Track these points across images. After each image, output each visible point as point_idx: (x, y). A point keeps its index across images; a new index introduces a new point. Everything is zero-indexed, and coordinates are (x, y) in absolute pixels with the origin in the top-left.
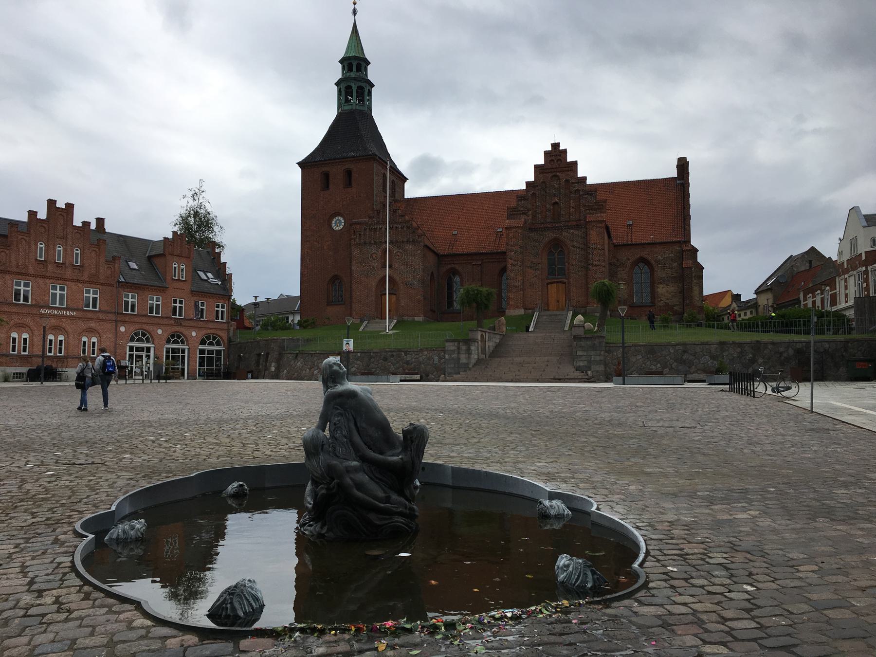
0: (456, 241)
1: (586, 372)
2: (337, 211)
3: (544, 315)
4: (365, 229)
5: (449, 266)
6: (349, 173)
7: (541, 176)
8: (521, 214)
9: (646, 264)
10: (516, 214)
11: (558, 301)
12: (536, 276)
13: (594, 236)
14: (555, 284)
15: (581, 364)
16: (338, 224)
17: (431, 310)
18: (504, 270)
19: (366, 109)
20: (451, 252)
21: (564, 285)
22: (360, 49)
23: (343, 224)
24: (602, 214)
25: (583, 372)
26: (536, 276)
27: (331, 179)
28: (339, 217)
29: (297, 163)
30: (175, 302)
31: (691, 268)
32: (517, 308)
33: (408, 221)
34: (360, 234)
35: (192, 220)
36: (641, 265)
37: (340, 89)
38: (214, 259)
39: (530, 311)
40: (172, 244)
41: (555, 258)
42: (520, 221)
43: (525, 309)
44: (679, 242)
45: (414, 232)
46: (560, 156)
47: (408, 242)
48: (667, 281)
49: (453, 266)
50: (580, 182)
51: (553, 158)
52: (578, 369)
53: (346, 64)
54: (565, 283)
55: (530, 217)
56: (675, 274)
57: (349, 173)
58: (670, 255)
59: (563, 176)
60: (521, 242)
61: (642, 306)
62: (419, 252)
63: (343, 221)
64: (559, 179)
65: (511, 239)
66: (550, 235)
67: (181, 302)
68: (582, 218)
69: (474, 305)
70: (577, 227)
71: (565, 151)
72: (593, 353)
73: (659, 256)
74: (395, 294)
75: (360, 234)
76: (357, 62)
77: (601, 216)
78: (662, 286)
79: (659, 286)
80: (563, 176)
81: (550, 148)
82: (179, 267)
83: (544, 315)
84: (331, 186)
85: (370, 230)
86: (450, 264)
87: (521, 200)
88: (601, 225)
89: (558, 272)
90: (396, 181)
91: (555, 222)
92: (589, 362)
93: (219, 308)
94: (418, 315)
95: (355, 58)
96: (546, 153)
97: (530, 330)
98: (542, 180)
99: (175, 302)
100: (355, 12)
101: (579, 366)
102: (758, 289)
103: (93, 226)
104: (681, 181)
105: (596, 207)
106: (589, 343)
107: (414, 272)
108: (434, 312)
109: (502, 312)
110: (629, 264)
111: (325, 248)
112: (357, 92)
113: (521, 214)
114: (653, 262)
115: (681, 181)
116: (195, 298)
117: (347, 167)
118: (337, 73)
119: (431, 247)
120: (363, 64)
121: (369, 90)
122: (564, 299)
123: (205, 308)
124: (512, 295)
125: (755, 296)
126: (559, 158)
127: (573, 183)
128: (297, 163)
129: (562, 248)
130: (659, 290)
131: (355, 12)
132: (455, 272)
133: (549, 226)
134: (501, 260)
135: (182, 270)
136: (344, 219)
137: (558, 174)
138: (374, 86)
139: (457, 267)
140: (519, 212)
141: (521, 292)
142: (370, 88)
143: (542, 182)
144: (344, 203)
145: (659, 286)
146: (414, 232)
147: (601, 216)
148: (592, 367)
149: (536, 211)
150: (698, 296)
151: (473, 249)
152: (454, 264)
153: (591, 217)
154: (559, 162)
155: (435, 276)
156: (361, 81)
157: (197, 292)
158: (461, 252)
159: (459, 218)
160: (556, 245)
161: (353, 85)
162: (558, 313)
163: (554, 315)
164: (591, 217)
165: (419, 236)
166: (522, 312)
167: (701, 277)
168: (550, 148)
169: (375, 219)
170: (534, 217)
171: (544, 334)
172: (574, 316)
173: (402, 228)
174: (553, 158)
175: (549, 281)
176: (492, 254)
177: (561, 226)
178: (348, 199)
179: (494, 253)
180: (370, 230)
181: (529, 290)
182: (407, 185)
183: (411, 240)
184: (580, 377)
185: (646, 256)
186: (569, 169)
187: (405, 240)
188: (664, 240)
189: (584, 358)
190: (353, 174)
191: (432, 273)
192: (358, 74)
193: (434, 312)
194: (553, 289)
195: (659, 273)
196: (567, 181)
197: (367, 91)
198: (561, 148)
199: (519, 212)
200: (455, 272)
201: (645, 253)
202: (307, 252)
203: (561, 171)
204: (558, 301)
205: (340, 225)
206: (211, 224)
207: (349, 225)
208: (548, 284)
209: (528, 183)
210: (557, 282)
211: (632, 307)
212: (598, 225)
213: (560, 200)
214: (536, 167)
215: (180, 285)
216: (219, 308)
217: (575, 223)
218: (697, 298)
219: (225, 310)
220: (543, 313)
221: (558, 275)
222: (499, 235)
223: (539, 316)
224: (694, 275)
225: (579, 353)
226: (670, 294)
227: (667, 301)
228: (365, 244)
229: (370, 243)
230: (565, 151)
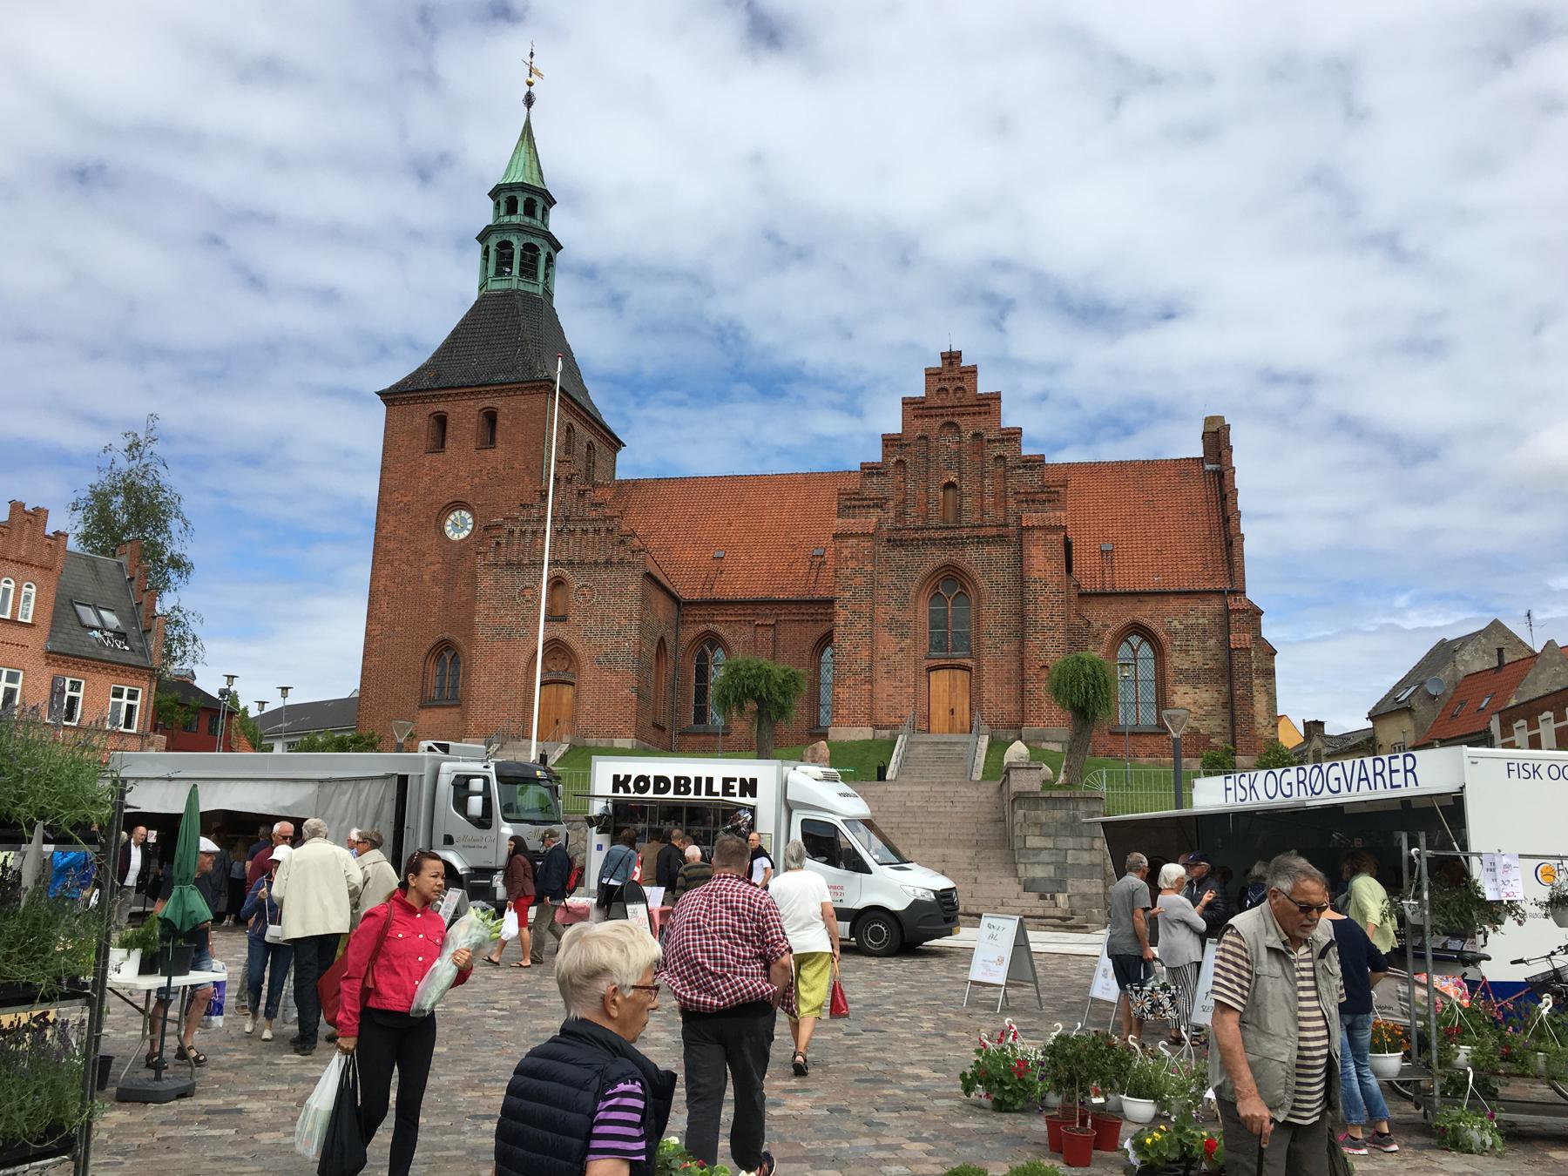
0: (721, 572)
1: (1053, 897)
2: (458, 499)
3: (921, 743)
4: (511, 532)
5: (702, 628)
6: (491, 417)
7: (917, 422)
8: (868, 506)
9: (1145, 639)
10: (859, 507)
11: (952, 711)
12: (902, 650)
13: (1042, 561)
14: (946, 672)
15: (1039, 872)
16: (458, 527)
17: (655, 725)
18: (826, 640)
19: (541, 292)
20: (707, 595)
21: (966, 674)
22: (535, 172)
23: (470, 527)
24: (1058, 514)
25: (1042, 897)
26: (902, 650)
27: (449, 430)
28: (463, 513)
29: (377, 393)
30: (118, 694)
31: (1248, 650)
32: (855, 724)
33: (612, 518)
34: (498, 543)
35: (119, 500)
36: (1135, 640)
37: (488, 247)
38: (131, 579)
39: (886, 733)
40: (53, 543)
41: (947, 610)
42: (869, 521)
43: (877, 727)
44: (1220, 593)
45: (622, 542)
46: (961, 379)
47: (608, 563)
48: (1193, 678)
49: (711, 626)
50: (1008, 440)
51: (945, 385)
52: (1029, 886)
53: (503, 199)
54: (969, 669)
55: (892, 514)
56: (1211, 664)
57: (491, 417)
58: (1200, 621)
59: (967, 425)
60: (869, 568)
61: (1140, 734)
62: (631, 588)
63: (470, 521)
64: (959, 432)
65: (846, 561)
66: (937, 557)
67: (132, 696)
68: (1011, 520)
69: (751, 706)
70: (1001, 539)
71: (973, 371)
72: (1071, 842)
73: (1176, 623)
74: (573, 684)
75: (498, 543)
76: (526, 195)
77: (1053, 516)
78: (1181, 689)
79: (1176, 689)
80: (967, 425)
81: (937, 363)
82: (18, 590)
83: (921, 743)
84: (448, 443)
85: (523, 533)
86: (705, 622)
87: (871, 475)
88: (1055, 537)
89: (952, 641)
90: (596, 444)
91: (948, 528)
92: (1061, 866)
93: (121, 696)
94: (620, 734)
95: (523, 187)
96: (930, 374)
97: (887, 777)
98: (919, 433)
99: (118, 694)
100: (529, 100)
101: (1033, 880)
102: (1375, 708)
103: (731, 791)
104: (1214, 467)
105: (1044, 496)
106: (1060, 814)
107: (619, 633)
108: (663, 729)
109: (817, 733)
110: (1107, 636)
111: (426, 578)
112: (523, 256)
113: (868, 506)
114: (1162, 635)
115: (1214, 467)
116: (54, 670)
117: (487, 403)
118: (484, 213)
119: (660, 576)
120: (540, 203)
121: (549, 254)
122: (967, 706)
123: (80, 695)
124: (844, 693)
125: (1370, 724)
126: (960, 384)
127: (989, 441)
128: (377, 393)
129: (963, 586)
130: (1175, 698)
131: (529, 100)
132: (714, 640)
133: (936, 535)
134: (819, 617)
135: (28, 598)
136: (474, 516)
137: (956, 420)
138: (562, 247)
139: (720, 629)
140: (865, 503)
141: (867, 687)
142: (553, 253)
143: (921, 438)
144: (476, 480)
145: (1176, 689)
146: (622, 542)
147: (1053, 516)
148: (1069, 881)
149: (904, 501)
150: (1265, 714)
151: (760, 590)
152: (713, 622)
153: (1031, 518)
154: (959, 394)
155: (668, 647)
156: (533, 235)
157: (61, 654)
158: (730, 595)
159: (730, 524)
160: (951, 580)
161: (514, 240)
162: (955, 738)
163: (945, 743)
164: (1031, 518)
165: (633, 552)
166: (866, 733)
167: (1270, 673)
168: (938, 363)
169: (535, 511)
170: (901, 515)
171: (925, 788)
172: (998, 746)
173: (597, 532)
174: (945, 385)
175: (935, 663)
176: (798, 602)
177: (962, 538)
178: (484, 472)
179: (806, 602)
180: (523, 533)
181: (885, 682)
182: (621, 456)
183: (615, 559)
184: (1040, 912)
185: (1146, 621)
186: (983, 409)
187: (602, 559)
188: (1186, 586)
189: (1044, 856)
190: (500, 420)
191: (662, 638)
192: (527, 219)
193: (663, 729)
194: (940, 680)
195: (1176, 660)
196: (977, 435)
197: (543, 259)
198: (962, 365)
199: (865, 503)
200: (714, 640)
201: (1144, 613)
202: (385, 587)
203: (964, 414)
204: (952, 711)
205: (463, 528)
206: (164, 512)
207: (485, 530)
208: (930, 669)
209: (889, 441)
210: (952, 667)
211: (1117, 734)
212: (1049, 537)
213: (960, 478)
214: (907, 402)
215: (12, 634)
216: (121, 696)
217: (994, 532)
218: (1261, 718)
219: (137, 703)
220: (918, 737)
221: (955, 649)
222: (817, 563)
223: (910, 744)
224: (1254, 667)
225: (1033, 842)
226: (1201, 707)
227: (1196, 724)
228: (509, 564)
229: (520, 564)
230: (973, 371)
